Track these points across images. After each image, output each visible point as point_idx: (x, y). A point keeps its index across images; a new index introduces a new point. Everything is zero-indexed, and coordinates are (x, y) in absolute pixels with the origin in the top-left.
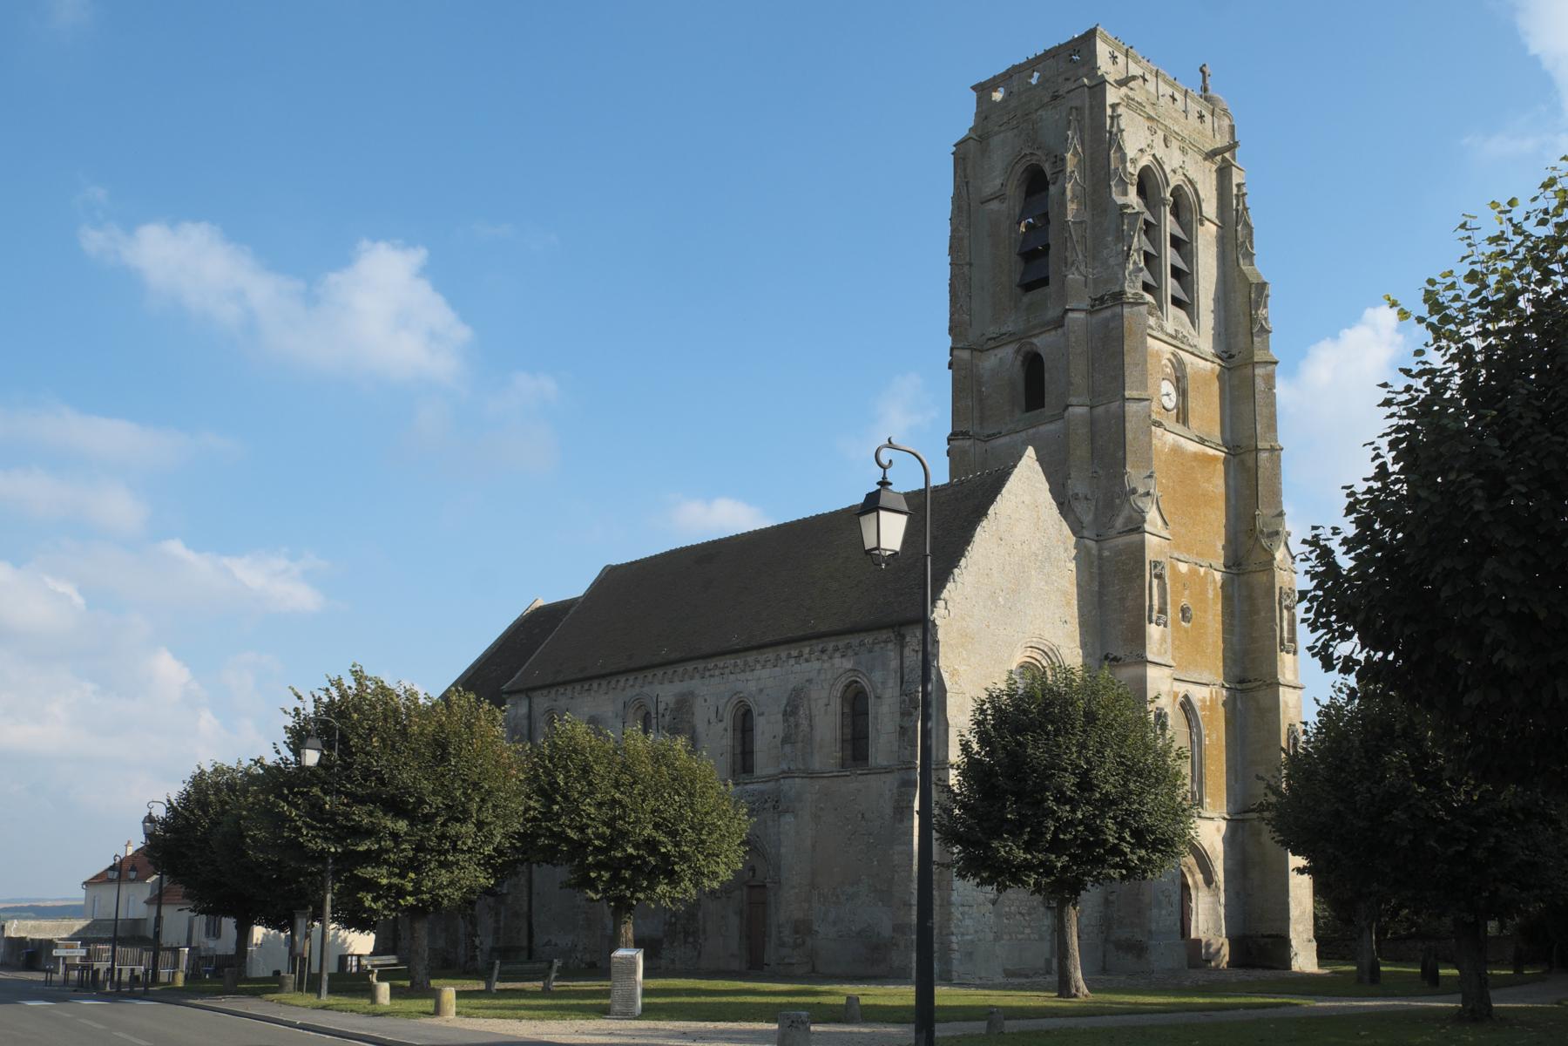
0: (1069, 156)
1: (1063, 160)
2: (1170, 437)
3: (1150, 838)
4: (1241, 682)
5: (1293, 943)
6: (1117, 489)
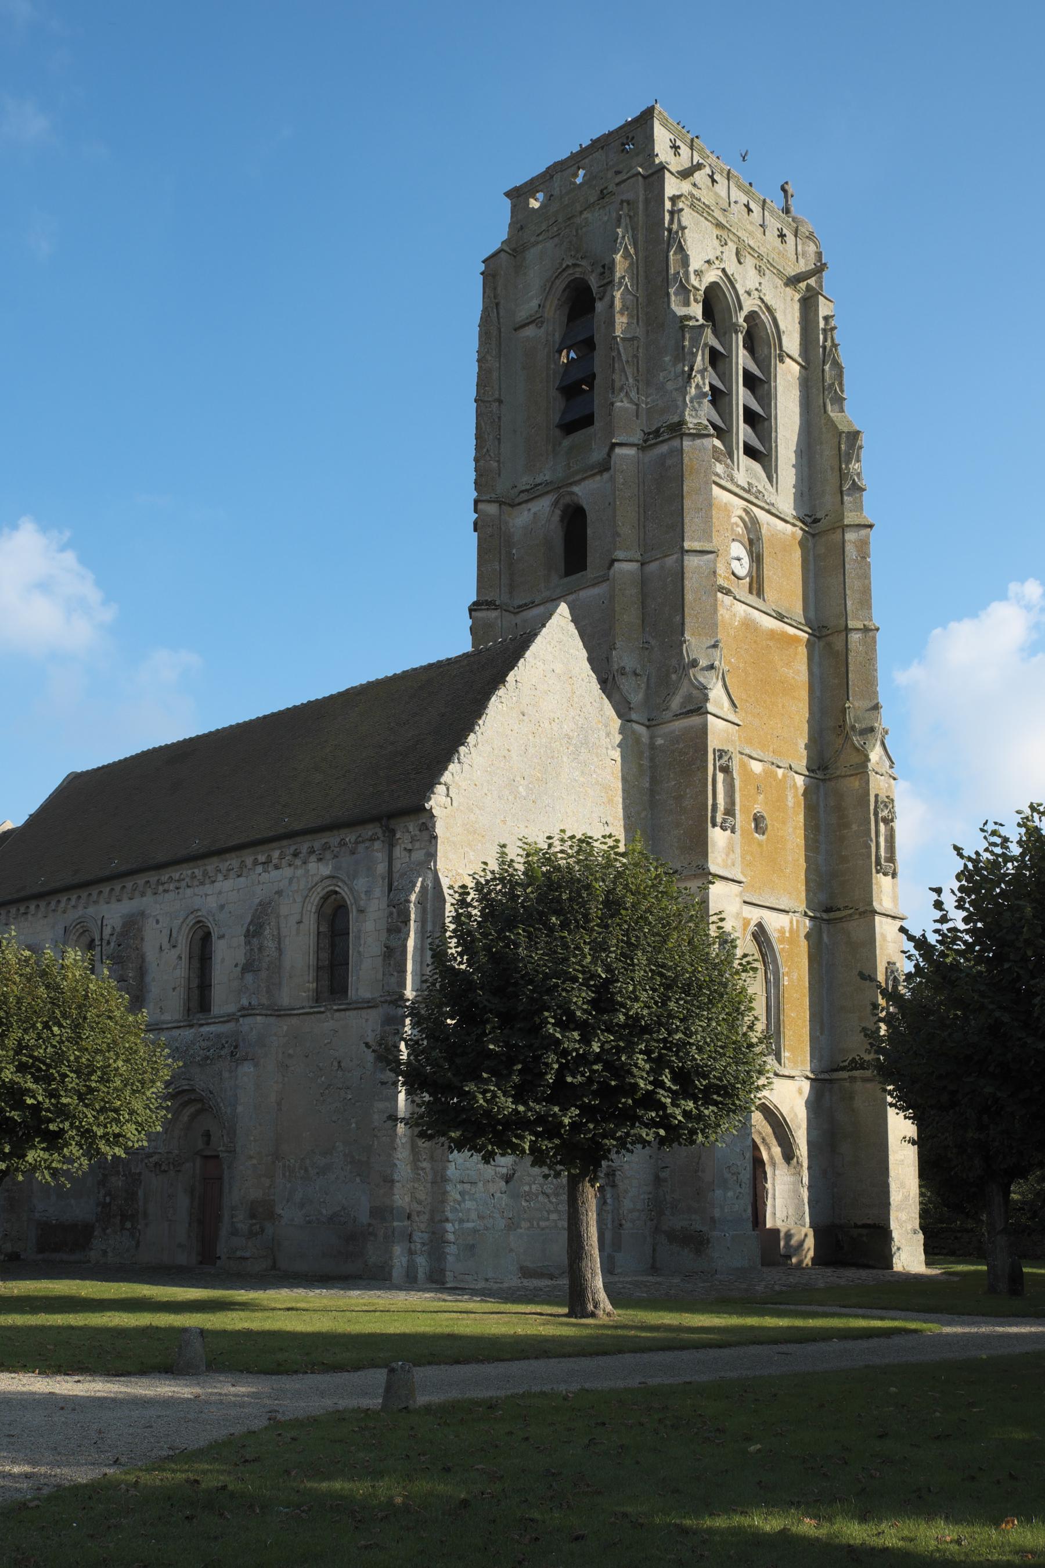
0: (618, 257)
1: (611, 267)
2: (740, 608)
3: (701, 1083)
4: (828, 910)
5: (895, 1235)
6: (674, 662)
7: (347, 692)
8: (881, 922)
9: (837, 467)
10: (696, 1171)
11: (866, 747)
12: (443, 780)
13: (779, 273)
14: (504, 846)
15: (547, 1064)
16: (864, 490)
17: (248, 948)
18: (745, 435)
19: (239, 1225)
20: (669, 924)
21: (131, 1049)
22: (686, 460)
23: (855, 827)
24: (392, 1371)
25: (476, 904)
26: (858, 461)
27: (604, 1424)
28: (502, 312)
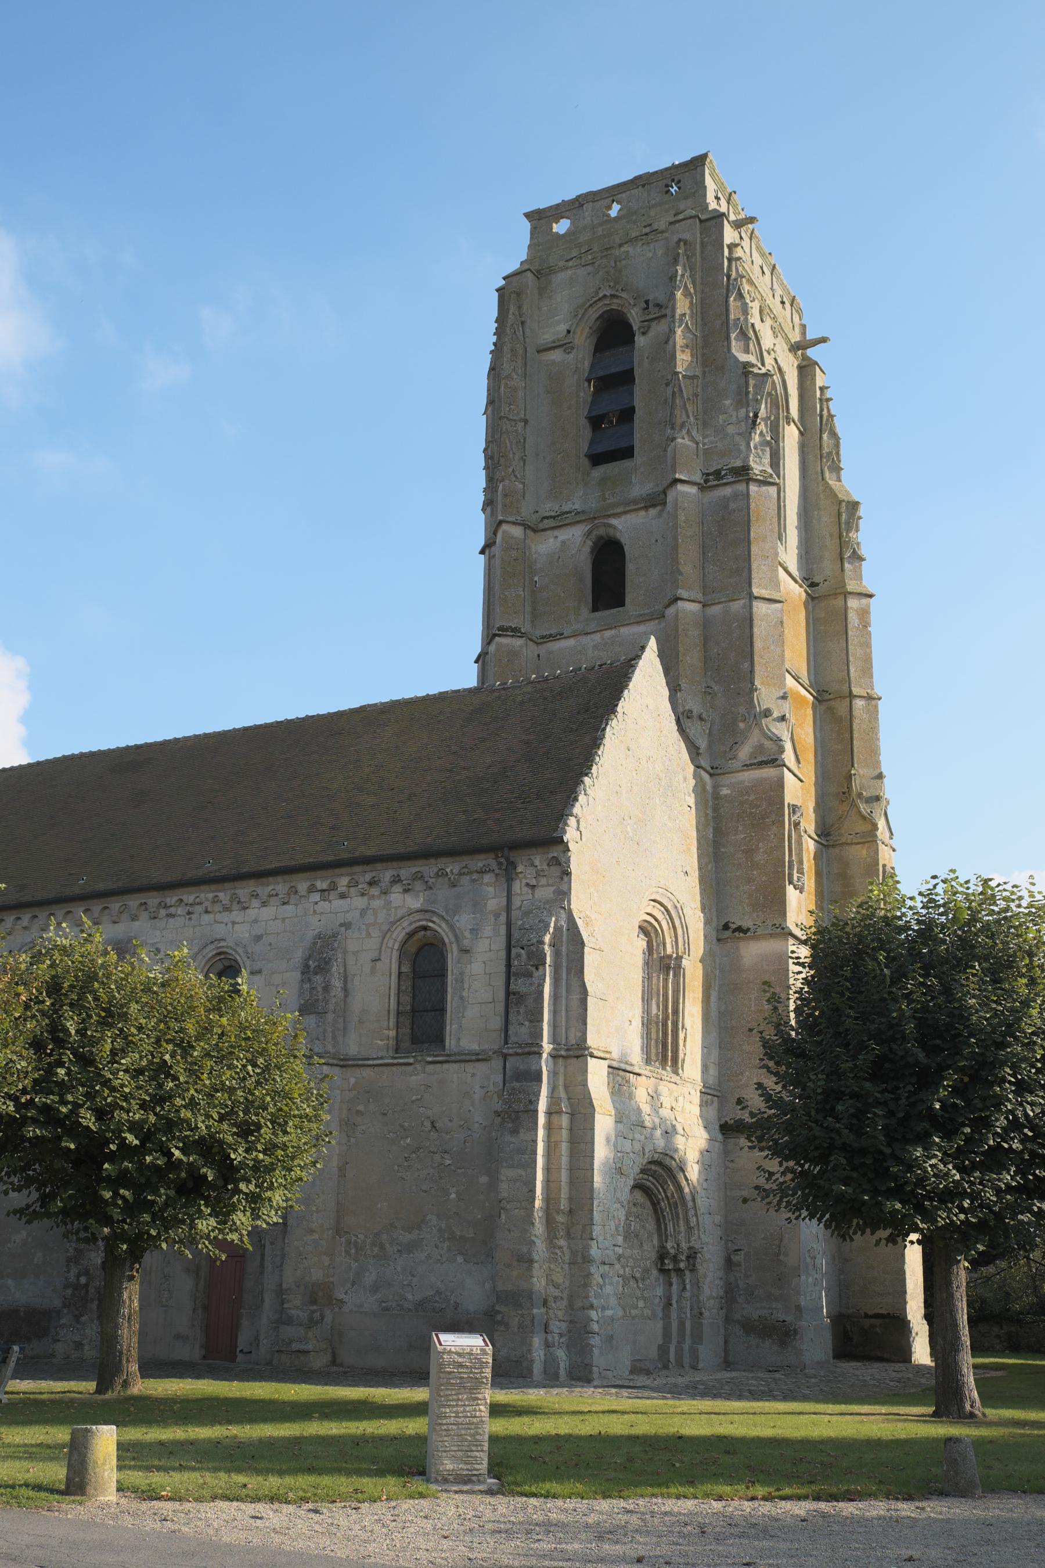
0: (679, 294)
6: (742, 709)
9: (836, 534)
10: (778, 1254)
11: (873, 815)
13: (787, 338)
16: (864, 560)
17: (307, 986)
19: (294, 1312)
22: (752, 506)
28: (527, 330)
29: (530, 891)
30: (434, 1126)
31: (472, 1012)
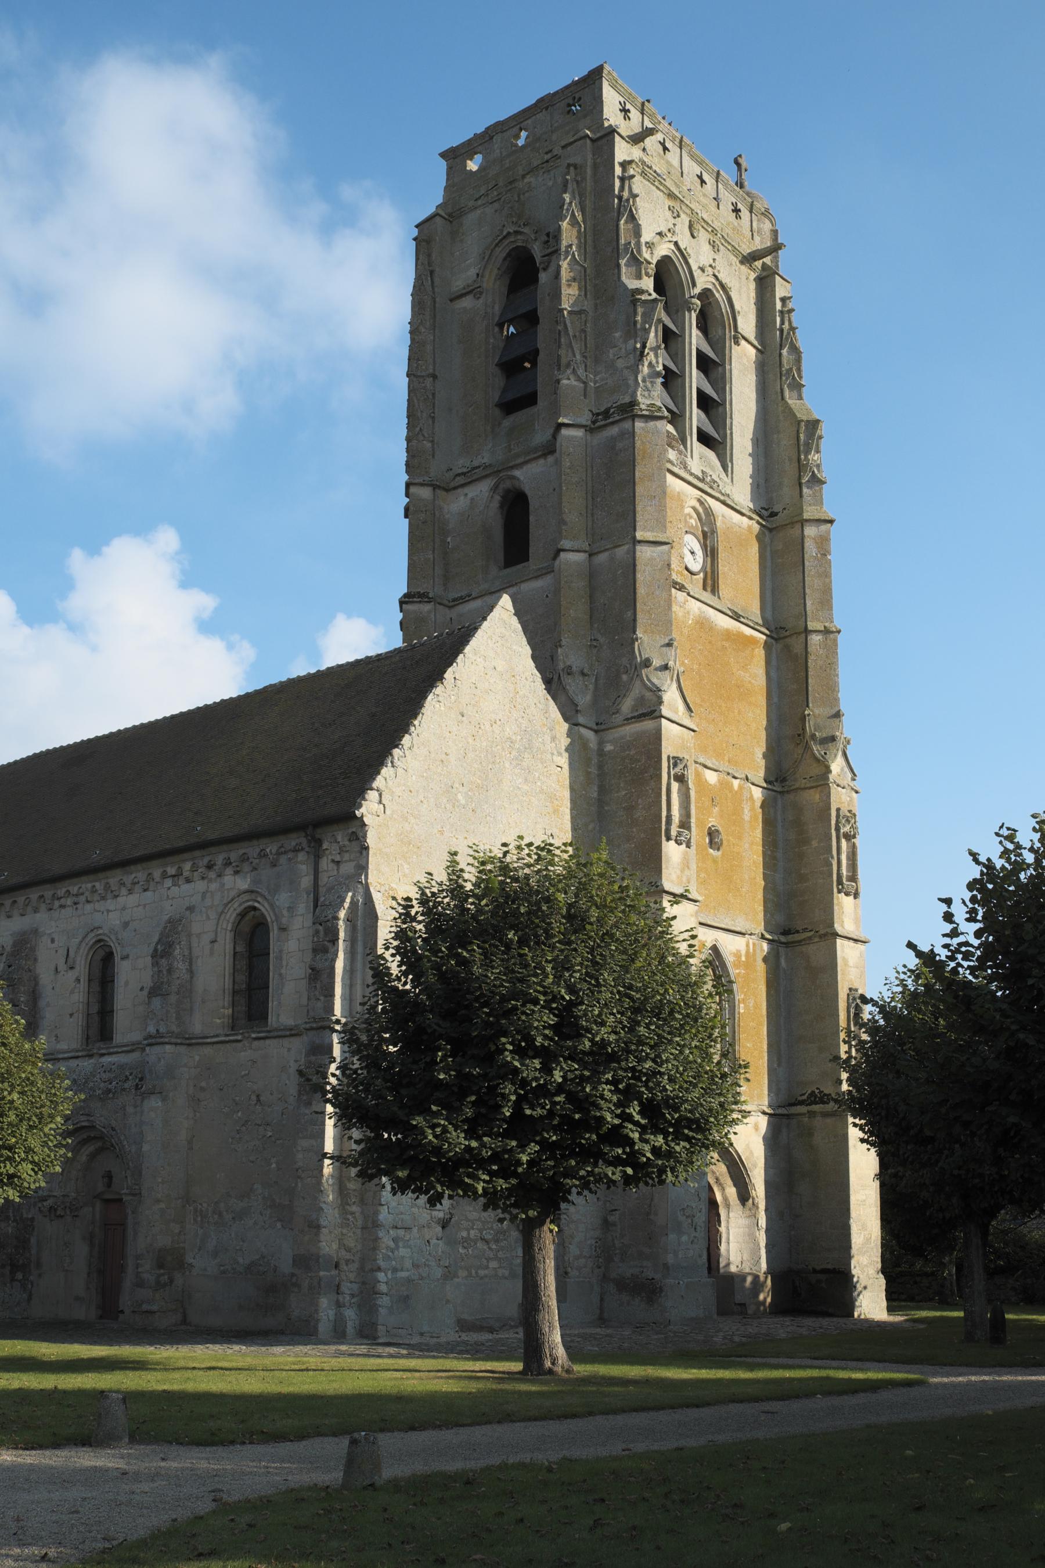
0: (565, 225)
2: (694, 606)
4: (786, 933)
6: (624, 661)
7: (265, 689)
8: (842, 945)
11: (827, 757)
12: (375, 785)
13: (735, 250)
14: (455, 854)
15: (503, 1096)
17: (156, 969)
18: (698, 421)
19: (145, 1276)
20: (636, 940)
21: (28, 1079)
22: (638, 444)
23: (815, 843)
24: (354, 1442)
25: (420, 918)
26: (818, 451)
27: (603, 1500)
28: (437, 280)
29: (335, 868)
30: (258, 1100)
31: (289, 988)
